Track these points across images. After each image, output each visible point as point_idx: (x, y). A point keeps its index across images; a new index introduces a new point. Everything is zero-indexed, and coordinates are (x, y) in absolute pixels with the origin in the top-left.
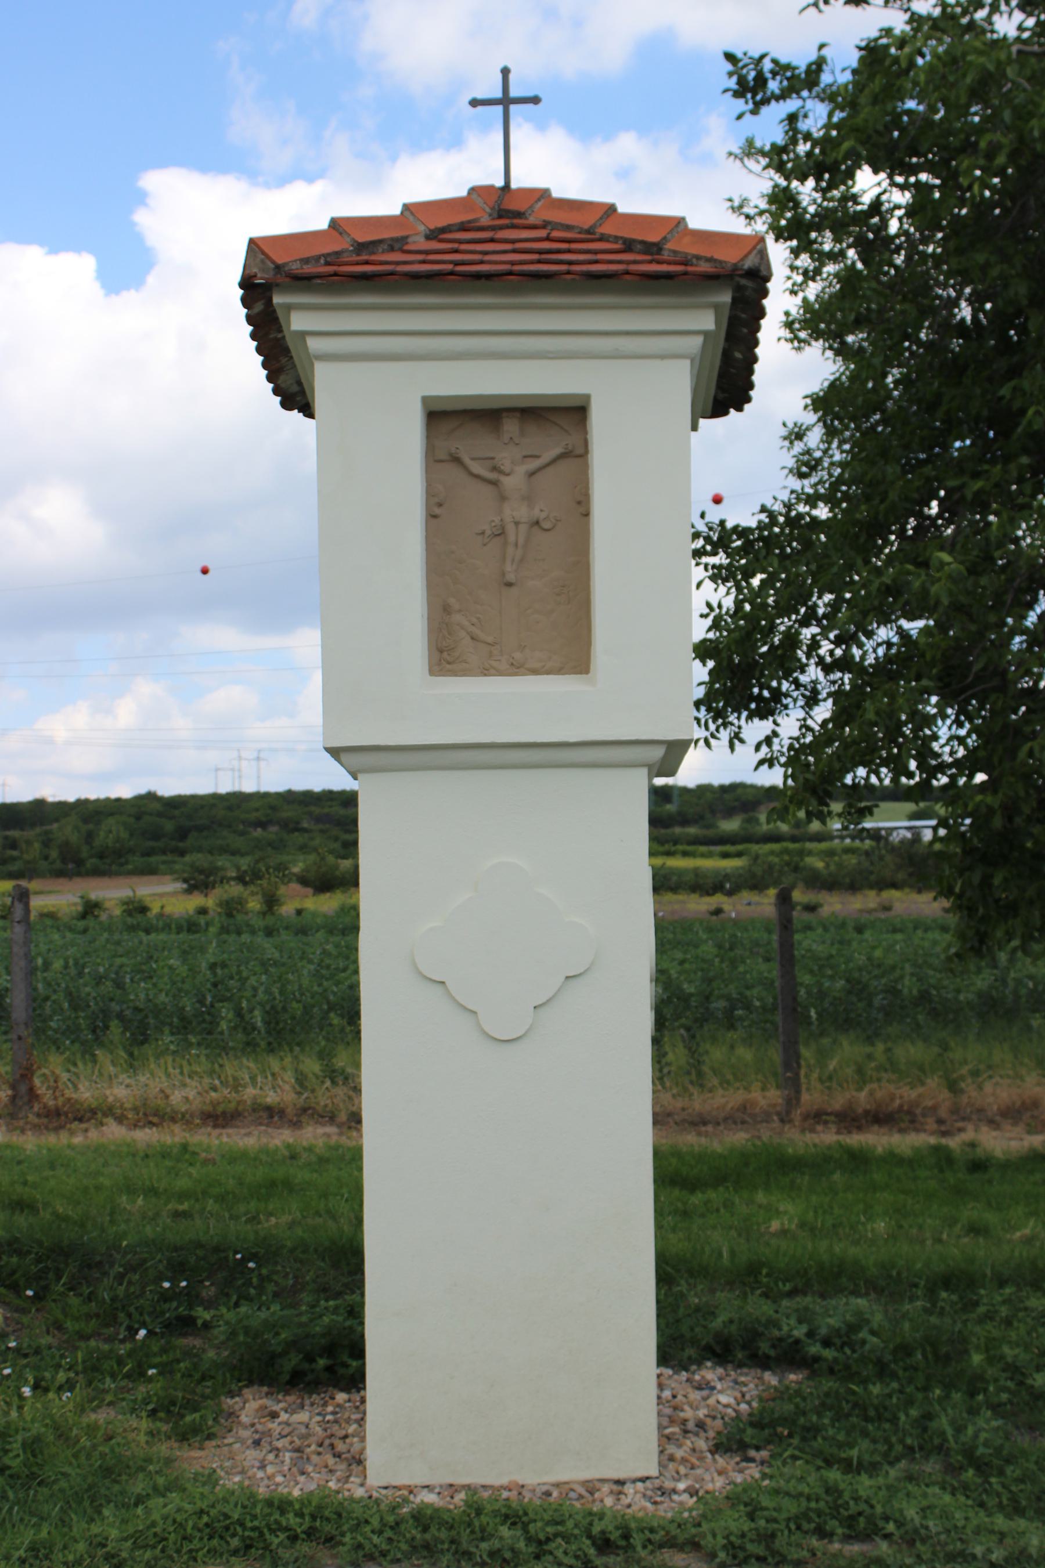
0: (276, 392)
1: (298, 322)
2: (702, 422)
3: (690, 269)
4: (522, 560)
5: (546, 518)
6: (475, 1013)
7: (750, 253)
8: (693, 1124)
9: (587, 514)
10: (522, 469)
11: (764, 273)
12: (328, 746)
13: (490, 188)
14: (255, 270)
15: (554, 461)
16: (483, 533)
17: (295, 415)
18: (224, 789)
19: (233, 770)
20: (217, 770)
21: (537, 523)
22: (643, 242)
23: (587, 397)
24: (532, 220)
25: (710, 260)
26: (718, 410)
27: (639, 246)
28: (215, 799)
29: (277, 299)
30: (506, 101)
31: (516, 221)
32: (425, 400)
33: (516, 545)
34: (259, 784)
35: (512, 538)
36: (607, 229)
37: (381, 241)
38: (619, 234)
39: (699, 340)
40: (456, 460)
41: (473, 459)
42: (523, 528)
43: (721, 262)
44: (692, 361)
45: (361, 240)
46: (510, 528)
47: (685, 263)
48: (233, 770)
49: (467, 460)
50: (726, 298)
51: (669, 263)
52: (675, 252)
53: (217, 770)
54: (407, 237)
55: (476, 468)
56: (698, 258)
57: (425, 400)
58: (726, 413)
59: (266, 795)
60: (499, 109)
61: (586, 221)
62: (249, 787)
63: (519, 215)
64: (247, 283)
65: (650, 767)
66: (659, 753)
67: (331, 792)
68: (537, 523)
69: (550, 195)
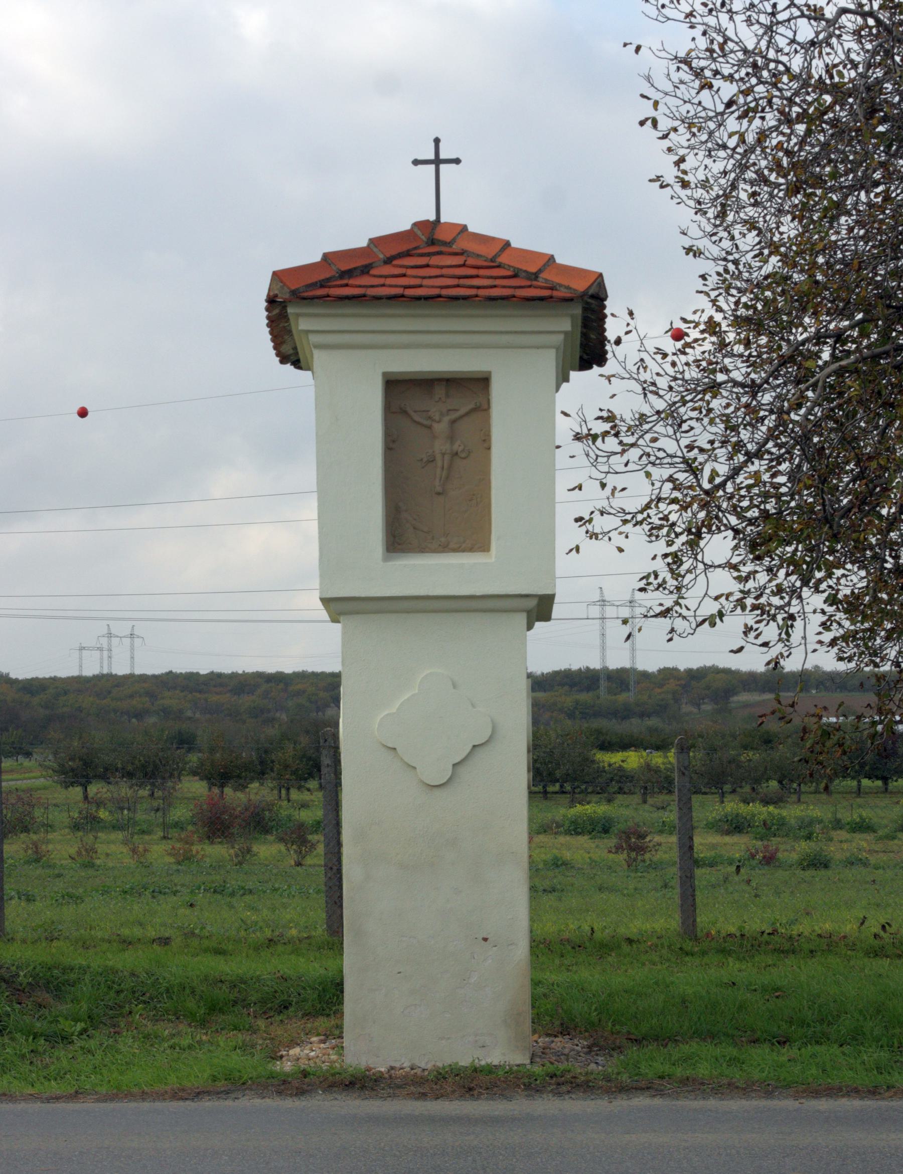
0: (277, 355)
1: (303, 324)
2: (574, 375)
3: (555, 293)
4: (447, 478)
5: (463, 451)
6: (415, 768)
7: (592, 284)
8: (565, 864)
9: (489, 448)
10: (446, 419)
11: (603, 296)
12: (324, 596)
13: (427, 222)
14: (276, 292)
15: (467, 414)
16: (422, 460)
17: (289, 367)
18: (90, 670)
19: (100, 649)
20: (82, 649)
21: (457, 454)
22: (525, 271)
23: (490, 373)
24: (455, 248)
25: (568, 288)
26: (585, 365)
27: (524, 274)
28: (79, 684)
29: (290, 310)
30: (437, 161)
31: (443, 249)
32: (385, 374)
33: (443, 468)
34: (132, 665)
35: (439, 463)
36: (503, 259)
37: (355, 269)
38: (512, 264)
39: (561, 337)
40: (405, 413)
41: (415, 412)
42: (447, 457)
43: (575, 290)
44: (557, 349)
45: (343, 269)
46: (439, 457)
47: (552, 289)
48: (100, 649)
49: (412, 414)
50: (578, 311)
51: (542, 288)
52: (546, 280)
53: (82, 649)
54: (371, 264)
55: (416, 417)
56: (561, 285)
57: (385, 374)
58: (590, 367)
59: (143, 678)
60: (433, 167)
61: (489, 252)
62: (121, 669)
63: (445, 244)
64: (271, 301)
65: (529, 612)
66: (533, 603)
67: (220, 675)
68: (457, 454)
69: (467, 230)
